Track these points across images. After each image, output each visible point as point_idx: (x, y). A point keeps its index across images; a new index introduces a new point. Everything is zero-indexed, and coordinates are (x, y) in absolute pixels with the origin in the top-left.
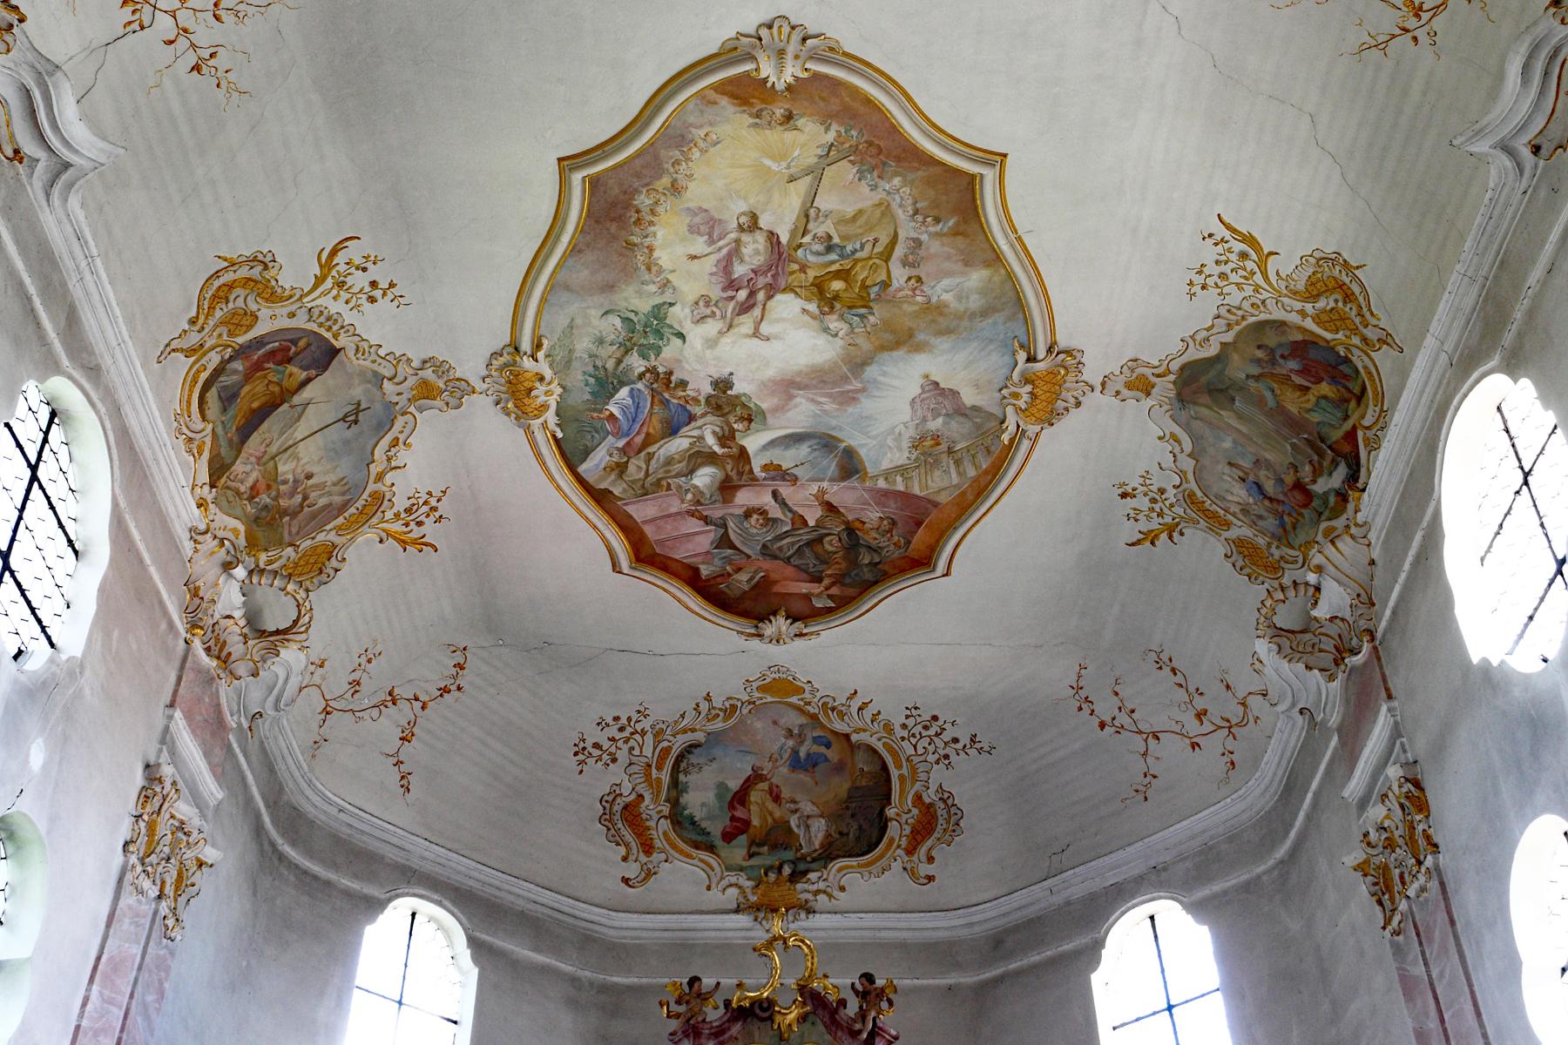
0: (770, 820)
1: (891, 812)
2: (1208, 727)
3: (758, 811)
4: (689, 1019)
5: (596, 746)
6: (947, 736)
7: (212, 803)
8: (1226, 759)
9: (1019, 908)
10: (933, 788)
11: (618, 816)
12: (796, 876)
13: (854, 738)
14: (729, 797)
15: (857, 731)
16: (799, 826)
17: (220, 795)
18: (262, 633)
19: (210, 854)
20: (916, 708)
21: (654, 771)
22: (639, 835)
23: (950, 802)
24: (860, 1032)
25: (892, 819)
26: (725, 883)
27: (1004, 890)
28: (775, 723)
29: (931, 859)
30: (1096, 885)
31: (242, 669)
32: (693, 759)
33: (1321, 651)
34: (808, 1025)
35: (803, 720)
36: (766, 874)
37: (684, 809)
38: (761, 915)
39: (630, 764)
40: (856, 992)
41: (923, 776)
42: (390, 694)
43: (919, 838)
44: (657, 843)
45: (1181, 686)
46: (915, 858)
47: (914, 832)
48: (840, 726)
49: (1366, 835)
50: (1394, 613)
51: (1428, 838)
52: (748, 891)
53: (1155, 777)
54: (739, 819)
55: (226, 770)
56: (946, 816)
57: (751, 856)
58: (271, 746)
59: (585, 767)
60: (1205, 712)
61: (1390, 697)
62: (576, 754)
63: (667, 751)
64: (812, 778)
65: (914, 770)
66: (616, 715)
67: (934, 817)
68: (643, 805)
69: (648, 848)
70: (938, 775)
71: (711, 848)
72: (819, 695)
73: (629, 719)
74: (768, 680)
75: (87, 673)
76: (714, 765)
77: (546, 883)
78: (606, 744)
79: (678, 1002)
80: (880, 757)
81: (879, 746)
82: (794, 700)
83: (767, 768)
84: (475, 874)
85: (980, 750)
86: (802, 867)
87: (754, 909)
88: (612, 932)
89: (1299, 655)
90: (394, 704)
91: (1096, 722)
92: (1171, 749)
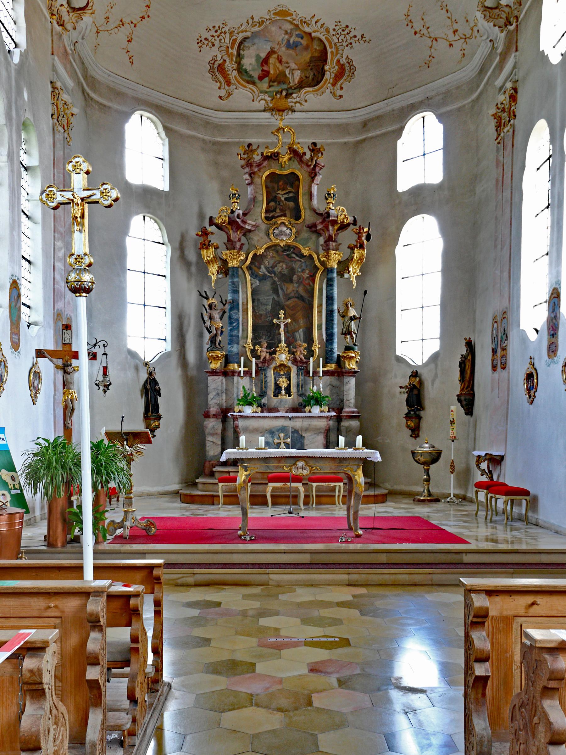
0: (278, 71)
1: (327, 68)
2: (457, 37)
3: (273, 67)
4: (248, 161)
5: (206, 39)
6: (352, 35)
7: (70, 88)
8: (462, 52)
9: (374, 111)
10: (345, 57)
11: (216, 70)
12: (288, 95)
13: (313, 35)
14: (261, 61)
15: (314, 32)
16: (289, 74)
17: (72, 84)
18: (74, 9)
19: (75, 110)
20: (340, 22)
21: (230, 50)
22: (225, 78)
23: (351, 63)
24: (310, 165)
25: (327, 71)
26: (259, 98)
27: (369, 103)
28: (280, 28)
29: (342, 88)
30: (404, 104)
31: (69, 26)
32: (246, 44)
33: (501, 18)
34: (292, 161)
35: (291, 27)
36: (276, 95)
37: (243, 66)
38: (274, 113)
39: (220, 47)
40: (310, 149)
41: (341, 52)
42: (121, 21)
43: (338, 79)
44: (232, 81)
45: (449, 18)
46: (335, 88)
47: (336, 76)
48: (307, 30)
49: (497, 104)
50: (526, 13)
51: (514, 112)
52: (269, 102)
53: (433, 57)
54: (265, 71)
55: (73, 74)
56: (349, 70)
57: (270, 86)
58: (82, 55)
59: (202, 49)
60: (457, 31)
61: (517, 50)
62: (198, 43)
63: (235, 40)
64: (295, 52)
65: (337, 49)
66: (214, 25)
67: (344, 69)
68: (226, 65)
69: (229, 83)
70: (347, 52)
71: (254, 83)
72: (299, 17)
73: (219, 27)
74: (277, 11)
75: (29, 53)
76: (255, 47)
77: (190, 100)
78: (210, 38)
79: (244, 154)
80: (323, 43)
81: (323, 38)
82: (288, 18)
83: (276, 48)
84: (162, 98)
85: (365, 41)
86: (290, 91)
87: (272, 110)
88: (217, 120)
89: (492, 19)
90: (123, 25)
91: (413, 31)
92: (442, 45)
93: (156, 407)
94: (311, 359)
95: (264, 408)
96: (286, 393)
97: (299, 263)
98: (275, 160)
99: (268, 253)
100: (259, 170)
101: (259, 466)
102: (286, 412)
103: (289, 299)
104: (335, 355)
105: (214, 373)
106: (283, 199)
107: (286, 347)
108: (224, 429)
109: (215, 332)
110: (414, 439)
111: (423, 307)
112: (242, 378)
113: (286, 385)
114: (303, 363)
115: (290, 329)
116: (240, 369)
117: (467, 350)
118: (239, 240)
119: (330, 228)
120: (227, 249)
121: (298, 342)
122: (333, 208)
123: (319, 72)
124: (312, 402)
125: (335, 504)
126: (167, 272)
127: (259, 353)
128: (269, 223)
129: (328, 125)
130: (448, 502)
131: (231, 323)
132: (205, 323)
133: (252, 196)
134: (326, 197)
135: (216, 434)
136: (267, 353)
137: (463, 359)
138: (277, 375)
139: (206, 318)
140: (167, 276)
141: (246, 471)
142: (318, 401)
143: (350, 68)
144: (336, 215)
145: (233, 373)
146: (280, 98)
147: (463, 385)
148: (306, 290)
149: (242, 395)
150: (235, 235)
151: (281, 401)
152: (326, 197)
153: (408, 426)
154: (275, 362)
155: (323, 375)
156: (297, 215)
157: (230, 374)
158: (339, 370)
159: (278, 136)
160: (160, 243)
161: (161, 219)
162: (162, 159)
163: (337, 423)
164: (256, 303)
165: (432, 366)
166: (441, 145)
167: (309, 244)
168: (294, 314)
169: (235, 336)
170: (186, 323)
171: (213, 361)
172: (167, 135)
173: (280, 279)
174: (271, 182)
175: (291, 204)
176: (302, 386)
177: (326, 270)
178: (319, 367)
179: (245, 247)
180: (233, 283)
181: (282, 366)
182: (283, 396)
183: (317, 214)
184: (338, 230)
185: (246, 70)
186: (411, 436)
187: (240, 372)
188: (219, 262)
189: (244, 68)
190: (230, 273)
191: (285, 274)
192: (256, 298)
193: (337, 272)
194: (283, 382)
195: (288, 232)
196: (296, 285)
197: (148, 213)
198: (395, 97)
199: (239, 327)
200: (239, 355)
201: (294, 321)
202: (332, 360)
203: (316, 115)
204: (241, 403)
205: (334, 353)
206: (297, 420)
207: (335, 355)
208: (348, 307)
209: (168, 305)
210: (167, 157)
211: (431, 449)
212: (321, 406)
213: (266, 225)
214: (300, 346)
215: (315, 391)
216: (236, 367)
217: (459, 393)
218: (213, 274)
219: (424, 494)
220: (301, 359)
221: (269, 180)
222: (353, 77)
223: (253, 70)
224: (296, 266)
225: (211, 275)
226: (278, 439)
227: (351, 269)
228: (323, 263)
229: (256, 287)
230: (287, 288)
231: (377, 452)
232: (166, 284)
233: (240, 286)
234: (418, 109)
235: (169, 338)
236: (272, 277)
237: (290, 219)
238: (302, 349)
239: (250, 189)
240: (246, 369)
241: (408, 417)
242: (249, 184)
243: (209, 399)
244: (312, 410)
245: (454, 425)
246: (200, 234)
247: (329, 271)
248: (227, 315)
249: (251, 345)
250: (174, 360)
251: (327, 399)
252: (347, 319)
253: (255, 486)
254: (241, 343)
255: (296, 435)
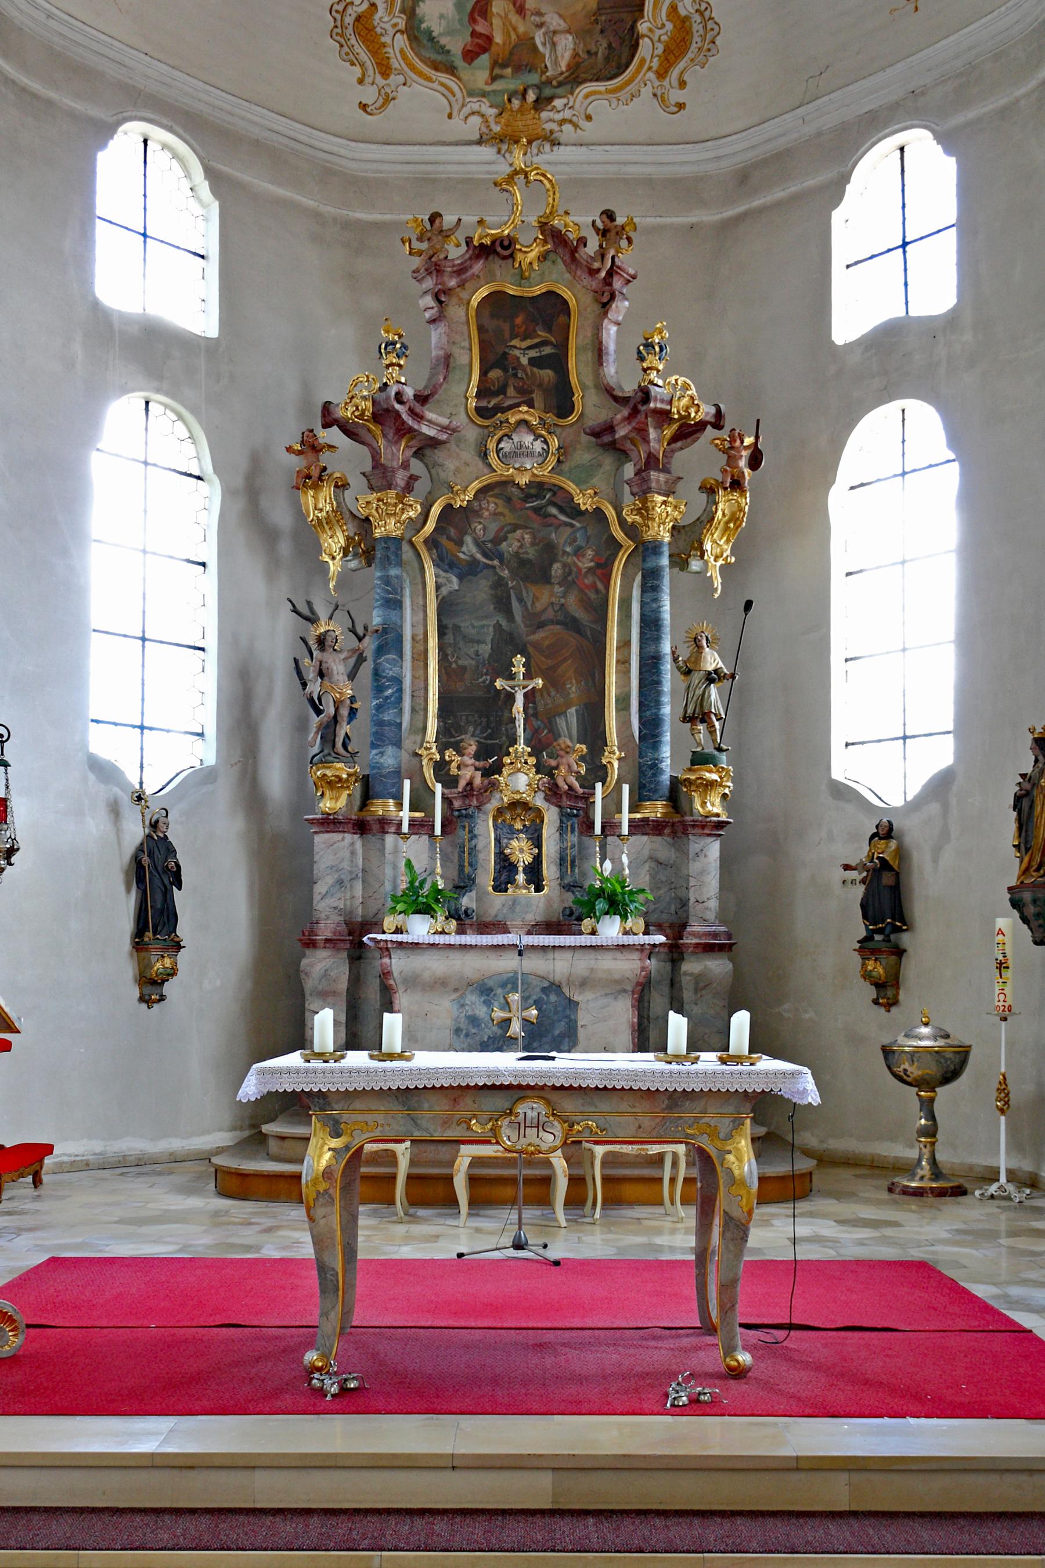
0: (514, 37)
1: (643, 27)
4: (431, 258)
11: (350, 30)
12: (542, 103)
16: (544, 44)
23: (707, 14)
24: (598, 271)
25: (644, 36)
26: (466, 110)
29: (682, 84)
34: (548, 263)
36: (509, 100)
37: (421, 22)
38: (504, 147)
40: (597, 230)
44: (395, 64)
46: (666, 83)
47: (667, 50)
52: (491, 120)
56: (701, 32)
57: (494, 78)
67: (689, 32)
68: (377, 17)
69: (385, 70)
71: (451, 70)
86: (547, 92)
93: (169, 917)
94: (599, 786)
95: (468, 921)
96: (529, 882)
97: (569, 530)
98: (505, 258)
99: (484, 504)
100: (462, 285)
101: (380, 1118)
102: (529, 933)
103: (541, 625)
104: (665, 778)
105: (330, 823)
106: (524, 361)
107: (530, 755)
108: (356, 981)
109: (332, 711)
110: (883, 1010)
111: (904, 650)
112: (405, 837)
113: (529, 859)
114: (577, 797)
115: (541, 708)
116: (401, 814)
117: (1036, 761)
118: (405, 465)
119: (653, 434)
120: (372, 488)
121: (561, 741)
122: (660, 383)
123: (622, 41)
124: (601, 905)
125: (661, 1203)
126: (210, 553)
127: (454, 770)
128: (486, 423)
129: (648, 182)
130: (992, 1197)
131: (379, 689)
132: (304, 685)
133: (441, 353)
134: (639, 352)
135: (334, 993)
136: (477, 769)
137: (1027, 786)
138: (504, 833)
139: (311, 674)
140: (208, 564)
141: (336, 1134)
142: (616, 905)
143: (705, 27)
144: (668, 398)
145: (384, 823)
146: (521, 110)
147: (1026, 859)
148: (586, 603)
149: (404, 886)
150: (396, 453)
151: (515, 902)
152: (639, 352)
153: (866, 975)
154: (498, 796)
155: (631, 833)
156: (564, 408)
157: (375, 827)
158: (677, 818)
159: (514, 195)
160: (190, 475)
161: (194, 411)
162: (202, 257)
163: (668, 966)
164: (449, 638)
165: (934, 808)
166: (950, 213)
167: (595, 481)
168: (554, 668)
169: (390, 724)
170: (260, 689)
171: (328, 793)
172: (215, 191)
173: (514, 574)
174: (493, 316)
175: (547, 375)
176: (573, 862)
177: (641, 549)
178: (620, 811)
179: (422, 486)
180: (387, 581)
181: (518, 806)
182: (521, 889)
183: (616, 399)
184: (674, 439)
185: (429, 33)
186: (876, 1002)
187: (400, 824)
188: (350, 526)
189: (424, 26)
190: (378, 554)
191: (529, 561)
192: (449, 622)
193: (670, 556)
194: (521, 852)
195: (538, 446)
196: (558, 589)
197: (158, 391)
198: (826, 98)
199: (400, 700)
200: (398, 775)
201: (553, 686)
202: (655, 791)
203: (616, 153)
204: (400, 907)
205: (661, 771)
206: (558, 954)
207: (665, 778)
208: (699, 647)
209: (212, 643)
210: (214, 251)
211: (941, 1042)
212: (624, 917)
213: (477, 430)
214: (568, 751)
215: (606, 874)
216: (392, 808)
217: (1013, 883)
218: (334, 558)
219: (920, 1173)
220: (570, 788)
221: (486, 312)
222: (714, 51)
223: (449, 32)
224: (560, 538)
225: (326, 558)
226: (502, 1009)
227: (708, 546)
228: (631, 531)
229: (451, 593)
230: (536, 598)
231: (805, 1070)
232: (209, 583)
233: (407, 592)
234: (885, 127)
235: (211, 732)
236: (494, 567)
237: (543, 415)
238: (572, 759)
239: (436, 335)
240: (417, 815)
241: (866, 948)
242: (433, 321)
243: (316, 898)
244: (599, 927)
245: (1008, 974)
246: (298, 447)
247: (648, 549)
248: (367, 668)
249: (434, 750)
250: (224, 793)
251: (640, 898)
252: (696, 678)
253: (423, 1147)
254: (408, 743)
255: (553, 998)
